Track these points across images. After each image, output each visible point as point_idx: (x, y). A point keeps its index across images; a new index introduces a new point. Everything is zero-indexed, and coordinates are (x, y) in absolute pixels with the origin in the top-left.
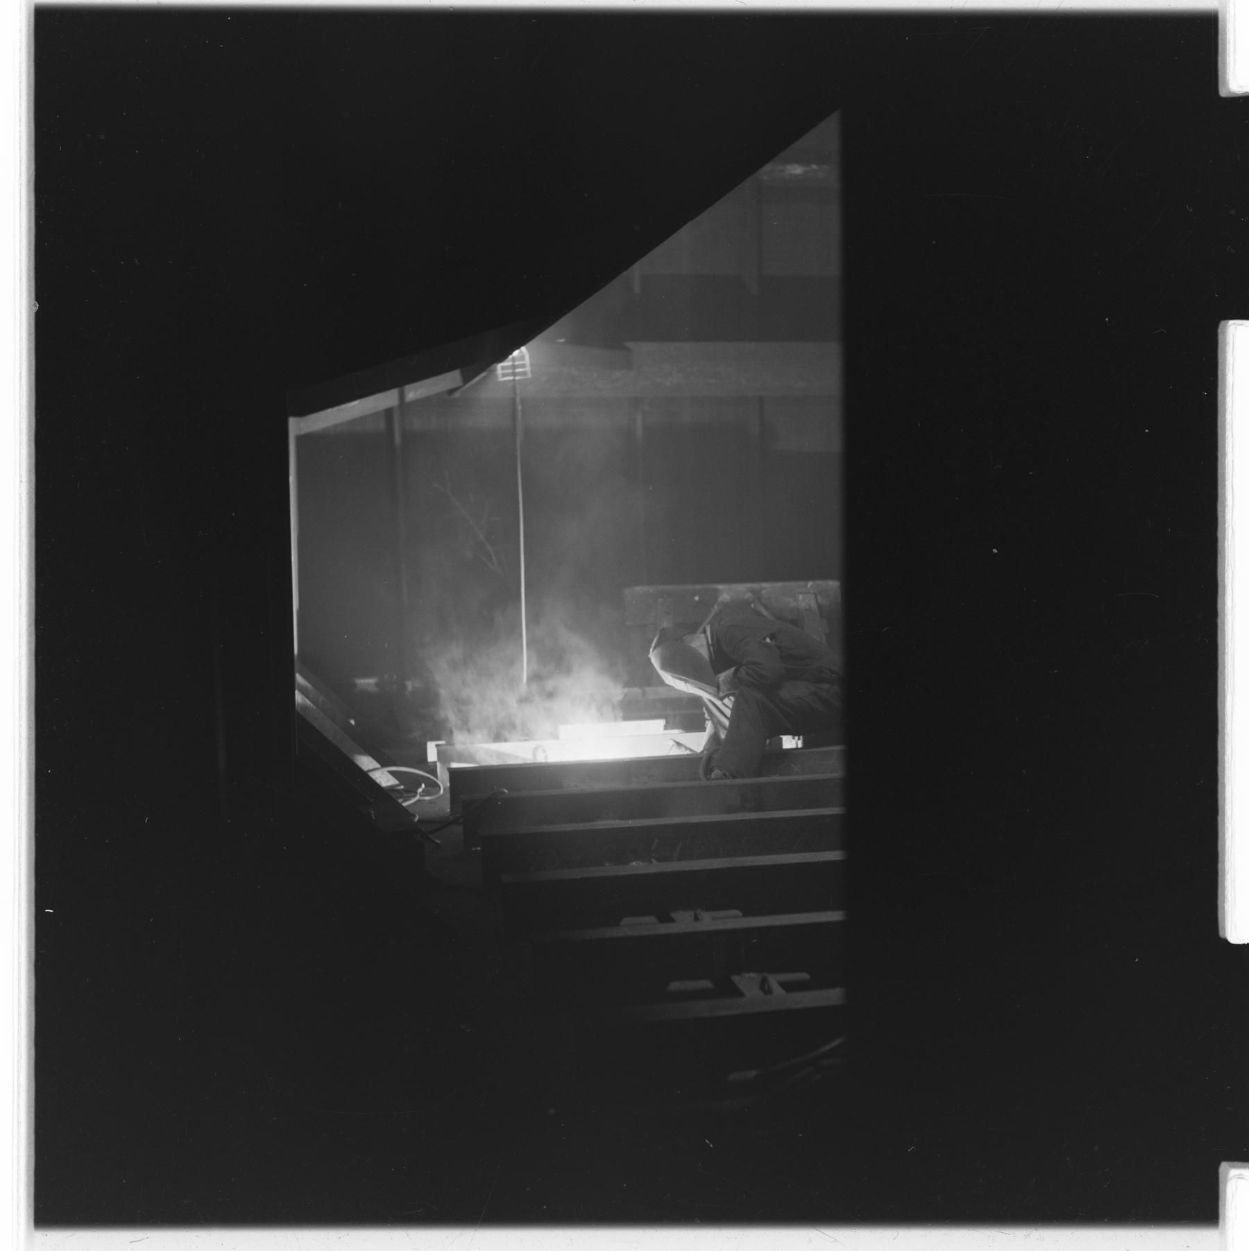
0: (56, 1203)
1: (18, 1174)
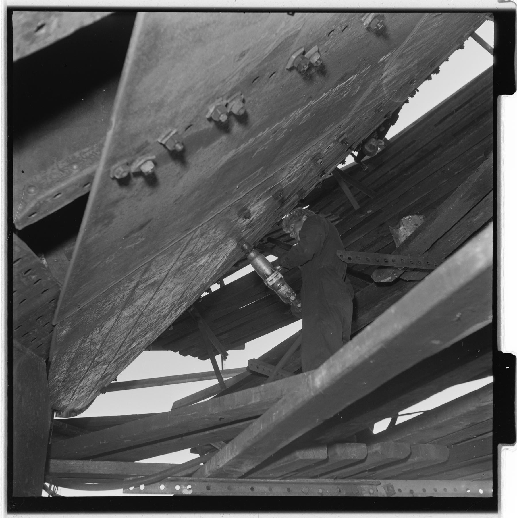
0: (14, 504)
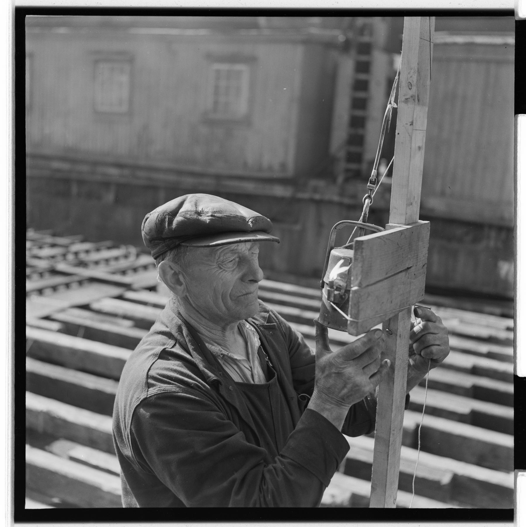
0: (20, 514)
1: (8, 473)
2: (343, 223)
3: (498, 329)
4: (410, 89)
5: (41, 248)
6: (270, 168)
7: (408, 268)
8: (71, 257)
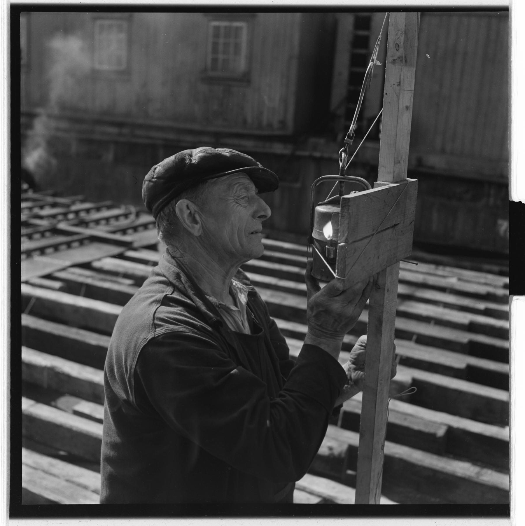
2: (359, 180)
3: (495, 286)
4: (397, 50)
5: (42, 207)
6: (270, 126)
7: (395, 225)
8: (71, 216)
